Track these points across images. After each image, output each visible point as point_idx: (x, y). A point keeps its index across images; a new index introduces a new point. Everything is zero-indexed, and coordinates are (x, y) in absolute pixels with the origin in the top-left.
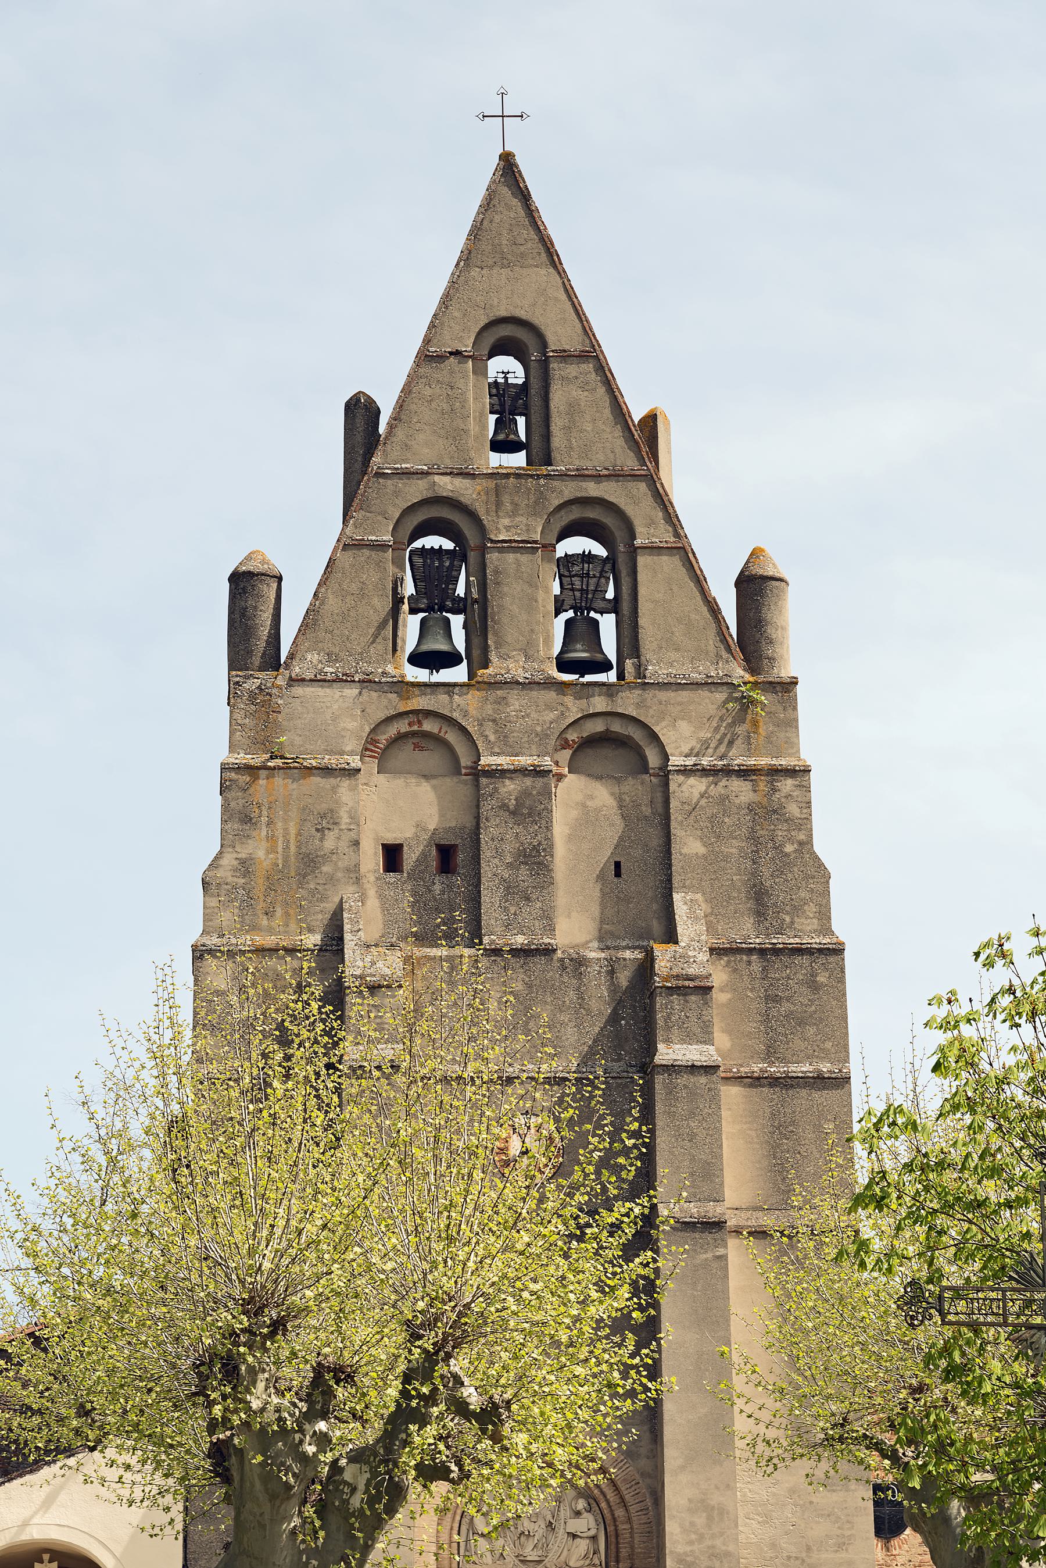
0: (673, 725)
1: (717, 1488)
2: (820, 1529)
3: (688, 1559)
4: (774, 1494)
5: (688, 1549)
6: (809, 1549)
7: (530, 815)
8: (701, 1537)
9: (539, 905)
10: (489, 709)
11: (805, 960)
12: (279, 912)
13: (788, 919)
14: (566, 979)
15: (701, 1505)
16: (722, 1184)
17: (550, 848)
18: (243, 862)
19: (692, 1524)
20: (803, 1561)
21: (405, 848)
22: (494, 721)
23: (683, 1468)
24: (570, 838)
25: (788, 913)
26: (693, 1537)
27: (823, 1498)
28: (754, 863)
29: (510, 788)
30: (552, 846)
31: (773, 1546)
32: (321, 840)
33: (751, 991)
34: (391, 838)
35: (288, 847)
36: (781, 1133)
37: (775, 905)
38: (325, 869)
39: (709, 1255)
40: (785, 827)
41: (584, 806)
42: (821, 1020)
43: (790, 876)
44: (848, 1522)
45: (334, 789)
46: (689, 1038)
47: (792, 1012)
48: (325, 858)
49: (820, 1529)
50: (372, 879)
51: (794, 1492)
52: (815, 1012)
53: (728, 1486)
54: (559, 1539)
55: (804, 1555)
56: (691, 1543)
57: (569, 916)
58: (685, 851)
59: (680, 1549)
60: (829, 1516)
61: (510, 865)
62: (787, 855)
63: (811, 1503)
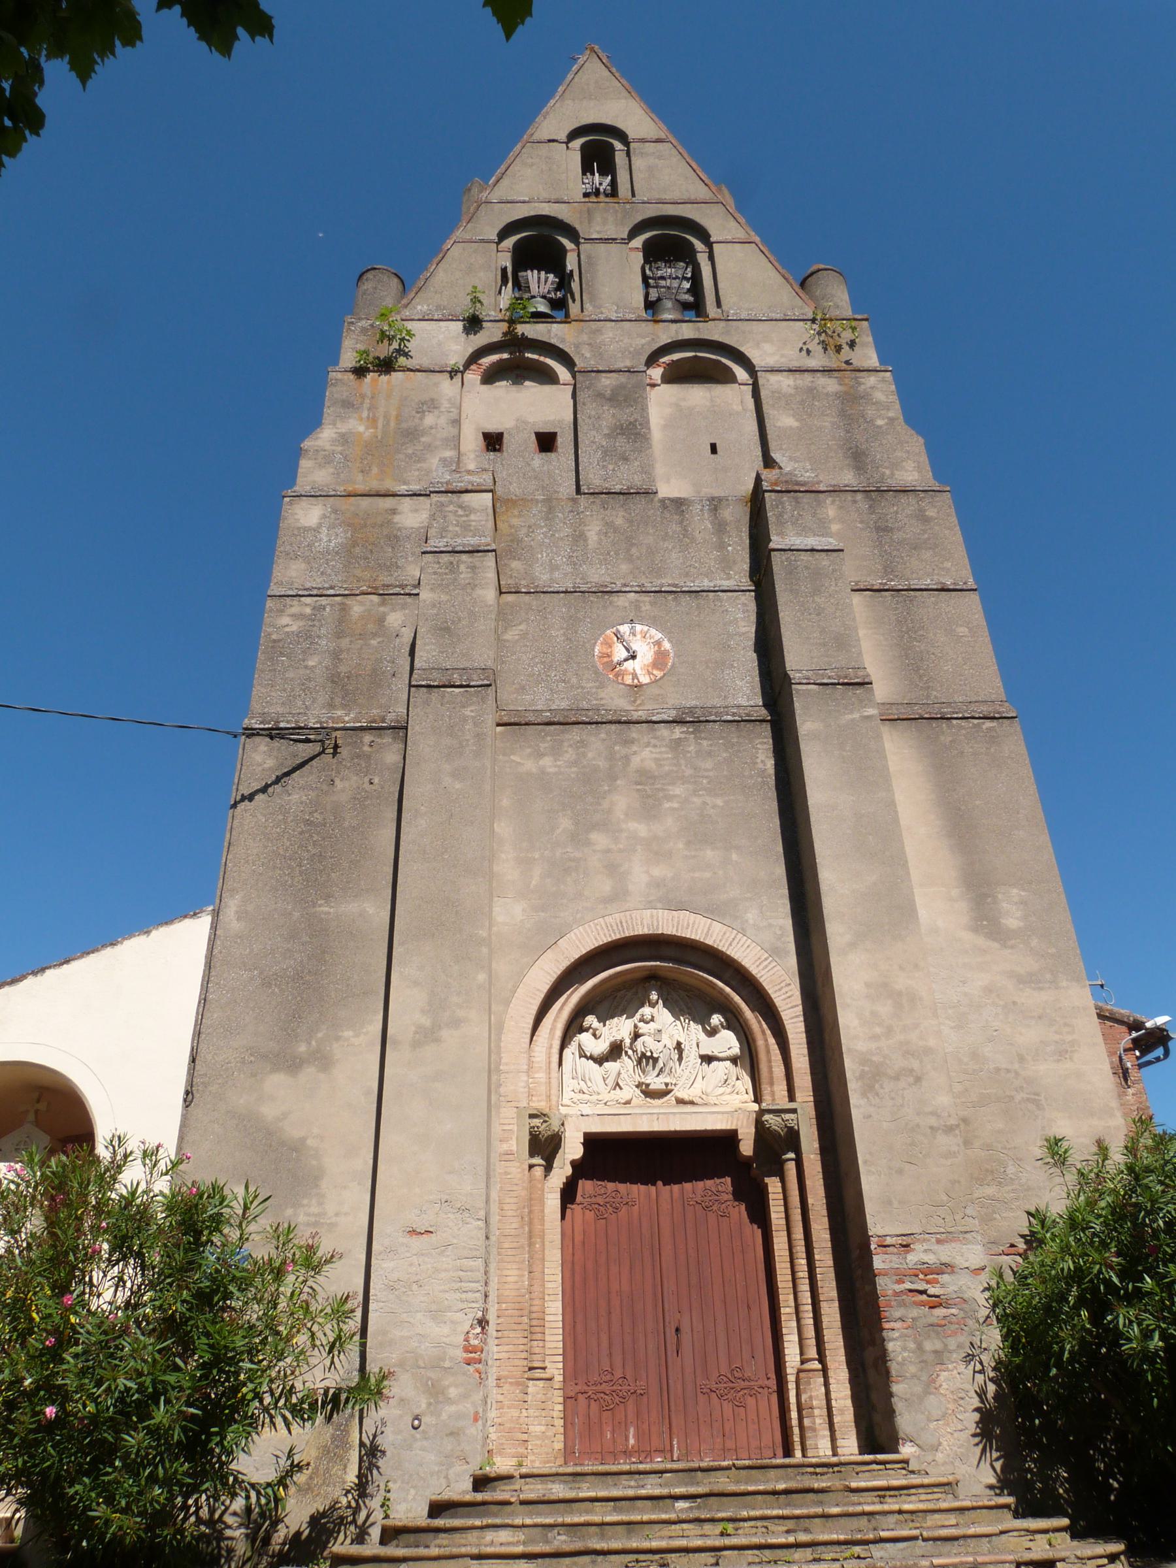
0: (758, 345)
1: (901, 968)
2: (1029, 1035)
3: (875, 1058)
4: (966, 994)
5: (873, 1045)
6: (1022, 1059)
7: (625, 401)
8: (889, 1031)
9: (637, 463)
10: (585, 338)
11: (912, 499)
12: (375, 470)
13: (888, 472)
14: (668, 515)
15: (883, 989)
16: (860, 654)
17: (646, 423)
18: (343, 435)
19: (874, 1014)
20: (1017, 1073)
21: (505, 436)
22: (589, 344)
23: (853, 945)
24: (665, 427)
25: (886, 468)
26: (878, 1030)
27: (1031, 998)
28: (848, 432)
29: (607, 382)
30: (648, 422)
31: (975, 1055)
32: (421, 419)
33: (861, 522)
34: (492, 427)
35: (388, 423)
36: (910, 637)
37: (873, 461)
38: (423, 439)
39: (856, 715)
40: (874, 407)
41: (677, 405)
42: (936, 546)
43: (884, 442)
44: (1066, 1025)
45: (436, 385)
46: (804, 531)
47: (905, 539)
48: (424, 433)
49: (1029, 1035)
50: (472, 456)
51: (990, 991)
52: (929, 539)
53: (916, 966)
54: (691, 1064)
55: (1016, 1066)
56: (875, 1037)
57: (668, 481)
58: (779, 424)
59: (861, 1046)
60: (1040, 1017)
61: (608, 436)
62: (880, 427)
63: (1014, 1003)
